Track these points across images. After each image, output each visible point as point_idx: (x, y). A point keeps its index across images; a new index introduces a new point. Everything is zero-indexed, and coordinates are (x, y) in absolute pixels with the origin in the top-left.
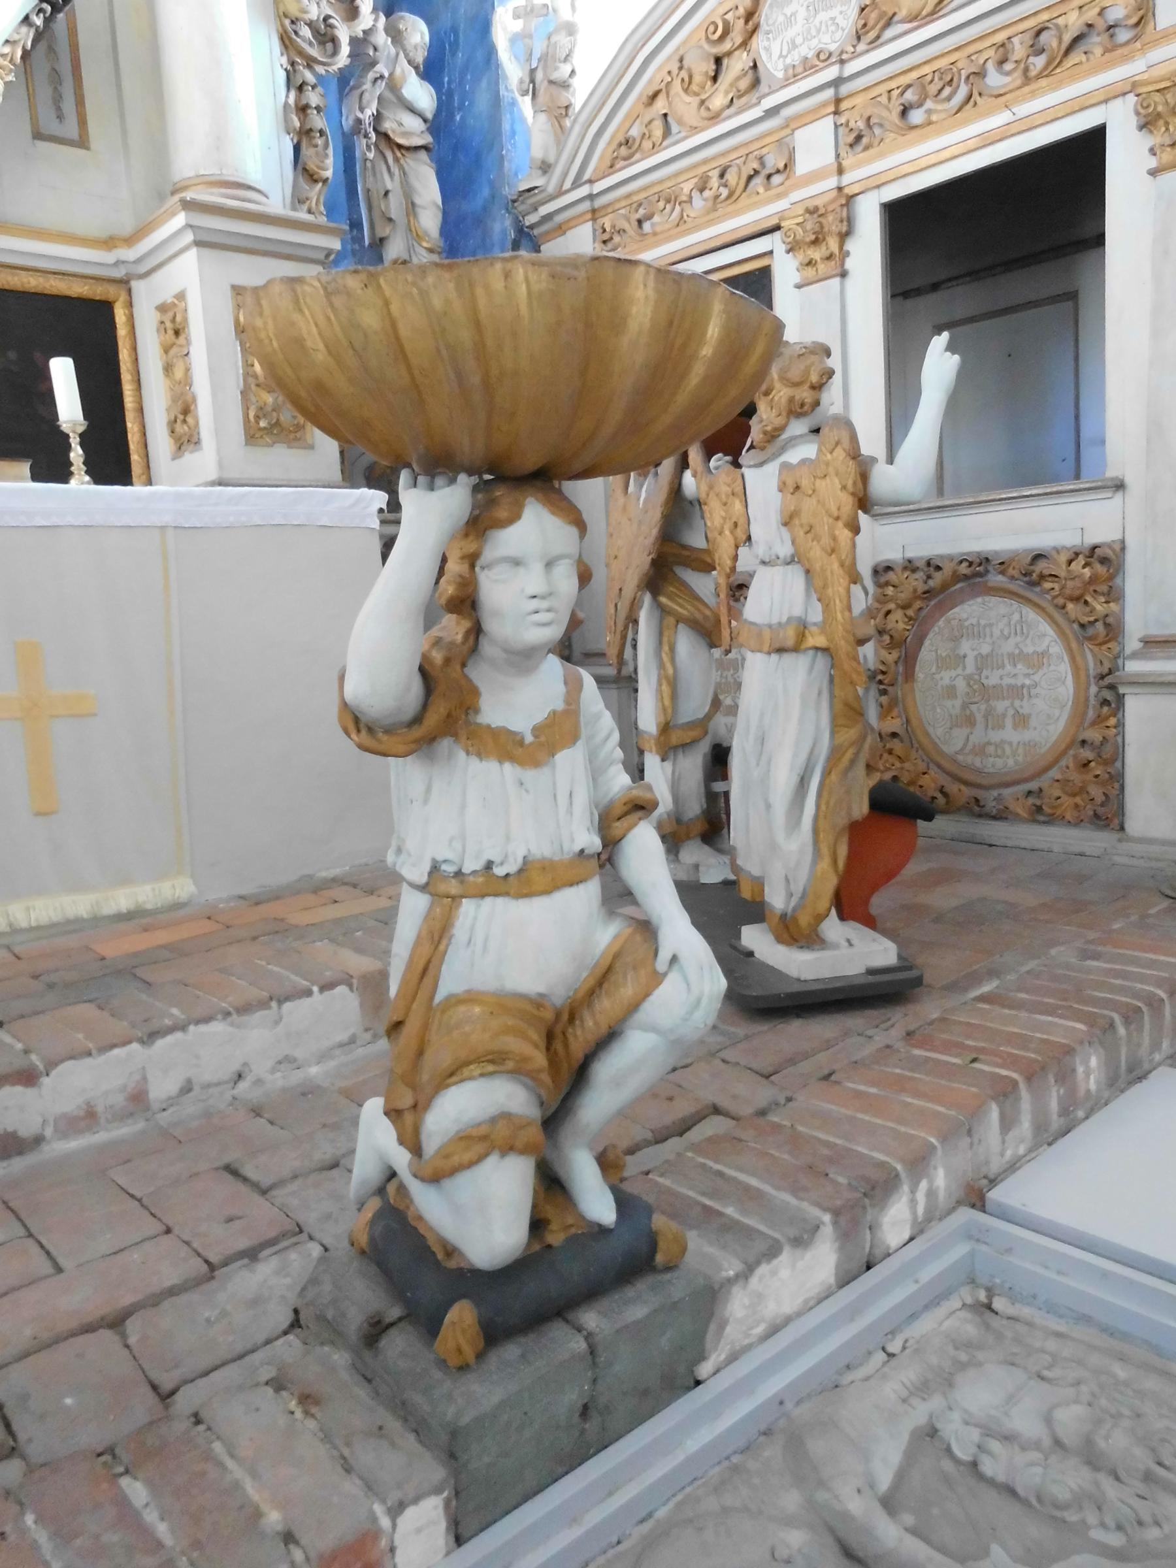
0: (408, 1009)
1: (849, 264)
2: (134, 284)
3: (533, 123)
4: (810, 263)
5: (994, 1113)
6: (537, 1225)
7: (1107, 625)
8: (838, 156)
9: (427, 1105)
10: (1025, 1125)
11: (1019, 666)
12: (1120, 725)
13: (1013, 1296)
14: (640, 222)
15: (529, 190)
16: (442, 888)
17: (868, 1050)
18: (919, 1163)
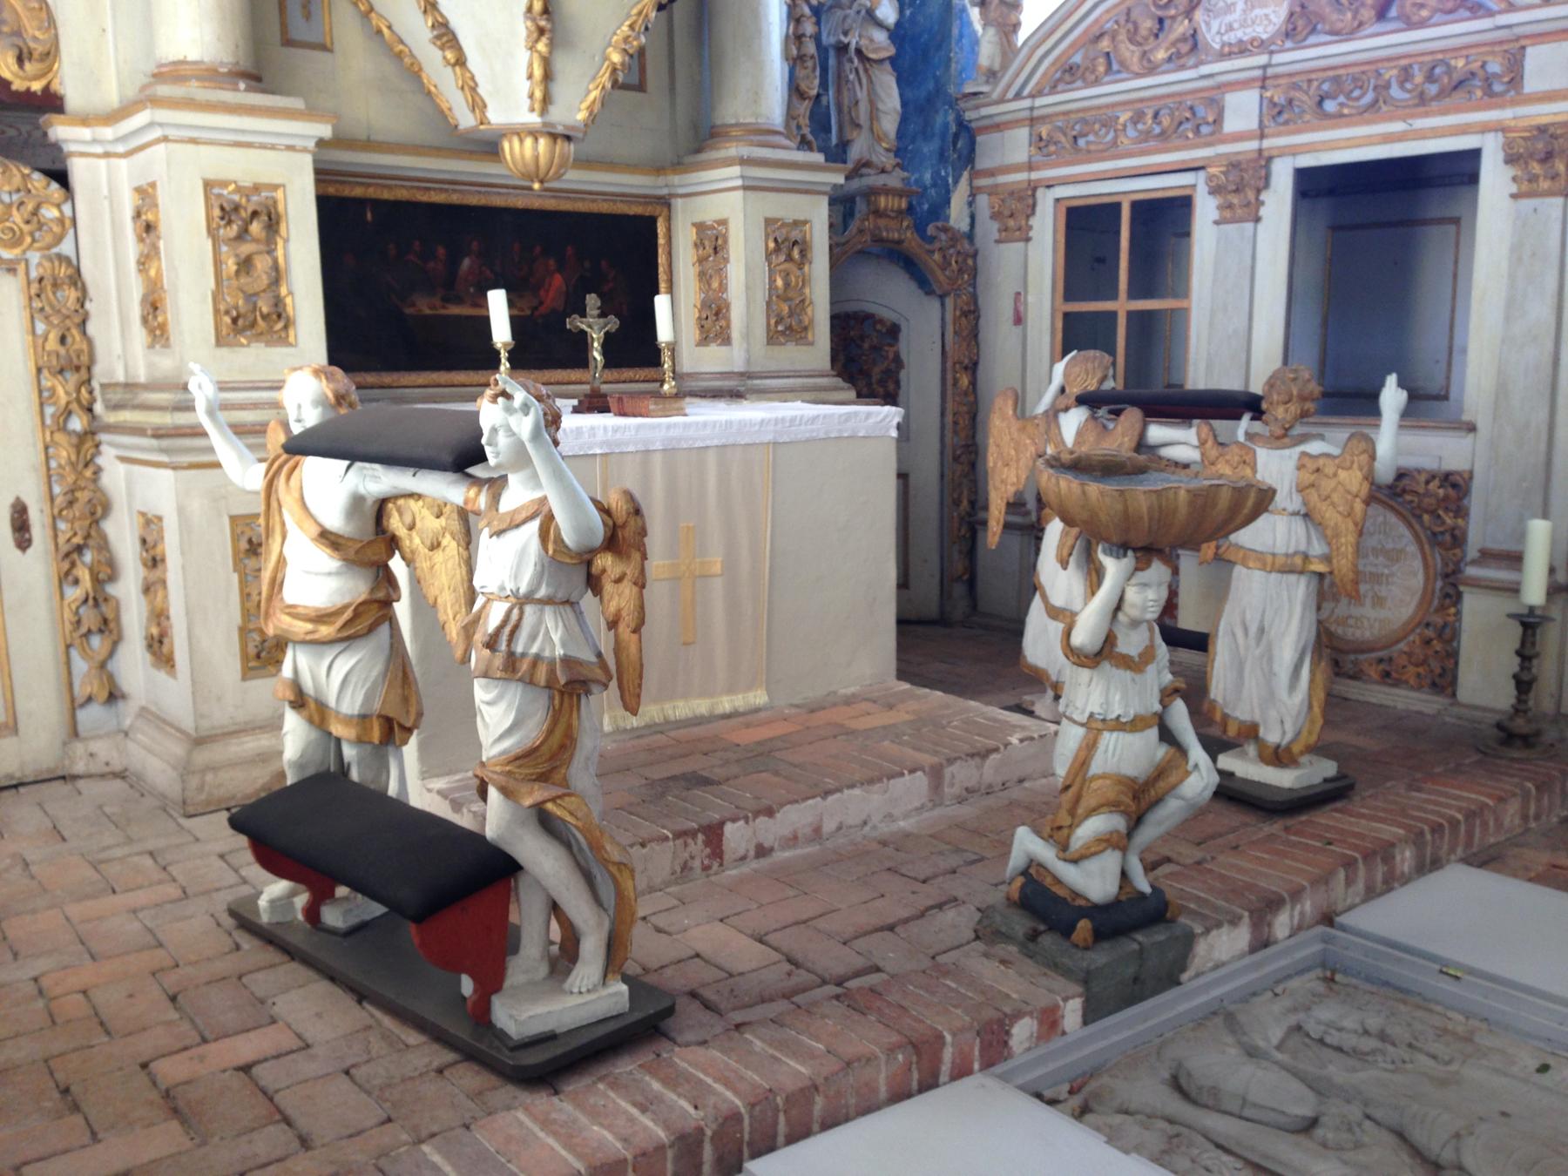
0: (1074, 781)
1: (1263, 212)
2: (673, 201)
3: (983, 35)
4: (1230, 206)
5: (1342, 874)
6: (1121, 888)
7: (1454, 537)
8: (1261, 122)
9: (1078, 825)
10: (1360, 886)
11: (1381, 559)
12: (1458, 613)
13: (1345, 972)
14: (1075, 138)
15: (975, 94)
16: (1094, 725)
17: (1261, 835)
18: (1296, 895)
